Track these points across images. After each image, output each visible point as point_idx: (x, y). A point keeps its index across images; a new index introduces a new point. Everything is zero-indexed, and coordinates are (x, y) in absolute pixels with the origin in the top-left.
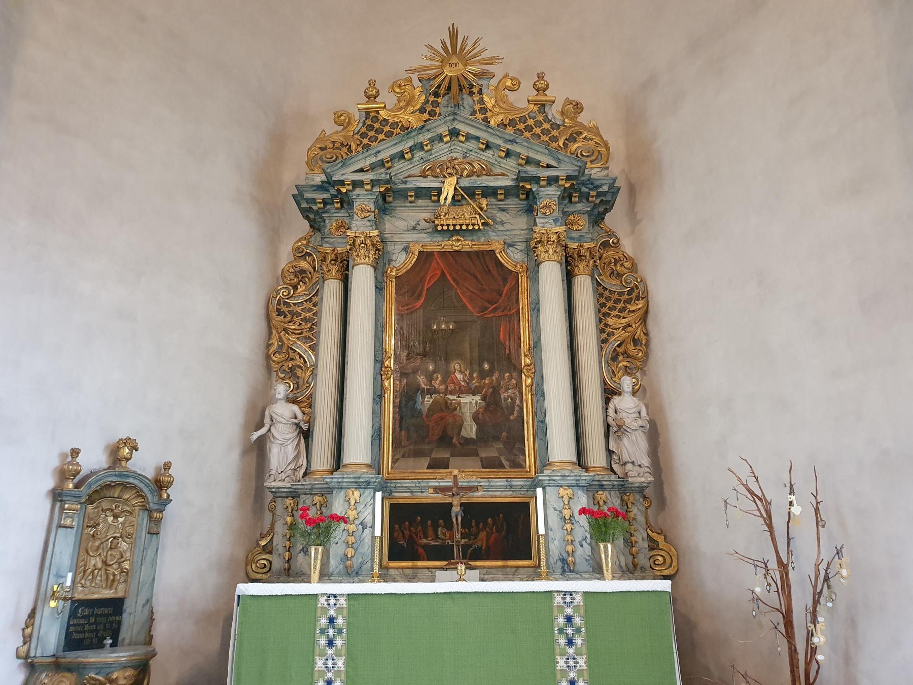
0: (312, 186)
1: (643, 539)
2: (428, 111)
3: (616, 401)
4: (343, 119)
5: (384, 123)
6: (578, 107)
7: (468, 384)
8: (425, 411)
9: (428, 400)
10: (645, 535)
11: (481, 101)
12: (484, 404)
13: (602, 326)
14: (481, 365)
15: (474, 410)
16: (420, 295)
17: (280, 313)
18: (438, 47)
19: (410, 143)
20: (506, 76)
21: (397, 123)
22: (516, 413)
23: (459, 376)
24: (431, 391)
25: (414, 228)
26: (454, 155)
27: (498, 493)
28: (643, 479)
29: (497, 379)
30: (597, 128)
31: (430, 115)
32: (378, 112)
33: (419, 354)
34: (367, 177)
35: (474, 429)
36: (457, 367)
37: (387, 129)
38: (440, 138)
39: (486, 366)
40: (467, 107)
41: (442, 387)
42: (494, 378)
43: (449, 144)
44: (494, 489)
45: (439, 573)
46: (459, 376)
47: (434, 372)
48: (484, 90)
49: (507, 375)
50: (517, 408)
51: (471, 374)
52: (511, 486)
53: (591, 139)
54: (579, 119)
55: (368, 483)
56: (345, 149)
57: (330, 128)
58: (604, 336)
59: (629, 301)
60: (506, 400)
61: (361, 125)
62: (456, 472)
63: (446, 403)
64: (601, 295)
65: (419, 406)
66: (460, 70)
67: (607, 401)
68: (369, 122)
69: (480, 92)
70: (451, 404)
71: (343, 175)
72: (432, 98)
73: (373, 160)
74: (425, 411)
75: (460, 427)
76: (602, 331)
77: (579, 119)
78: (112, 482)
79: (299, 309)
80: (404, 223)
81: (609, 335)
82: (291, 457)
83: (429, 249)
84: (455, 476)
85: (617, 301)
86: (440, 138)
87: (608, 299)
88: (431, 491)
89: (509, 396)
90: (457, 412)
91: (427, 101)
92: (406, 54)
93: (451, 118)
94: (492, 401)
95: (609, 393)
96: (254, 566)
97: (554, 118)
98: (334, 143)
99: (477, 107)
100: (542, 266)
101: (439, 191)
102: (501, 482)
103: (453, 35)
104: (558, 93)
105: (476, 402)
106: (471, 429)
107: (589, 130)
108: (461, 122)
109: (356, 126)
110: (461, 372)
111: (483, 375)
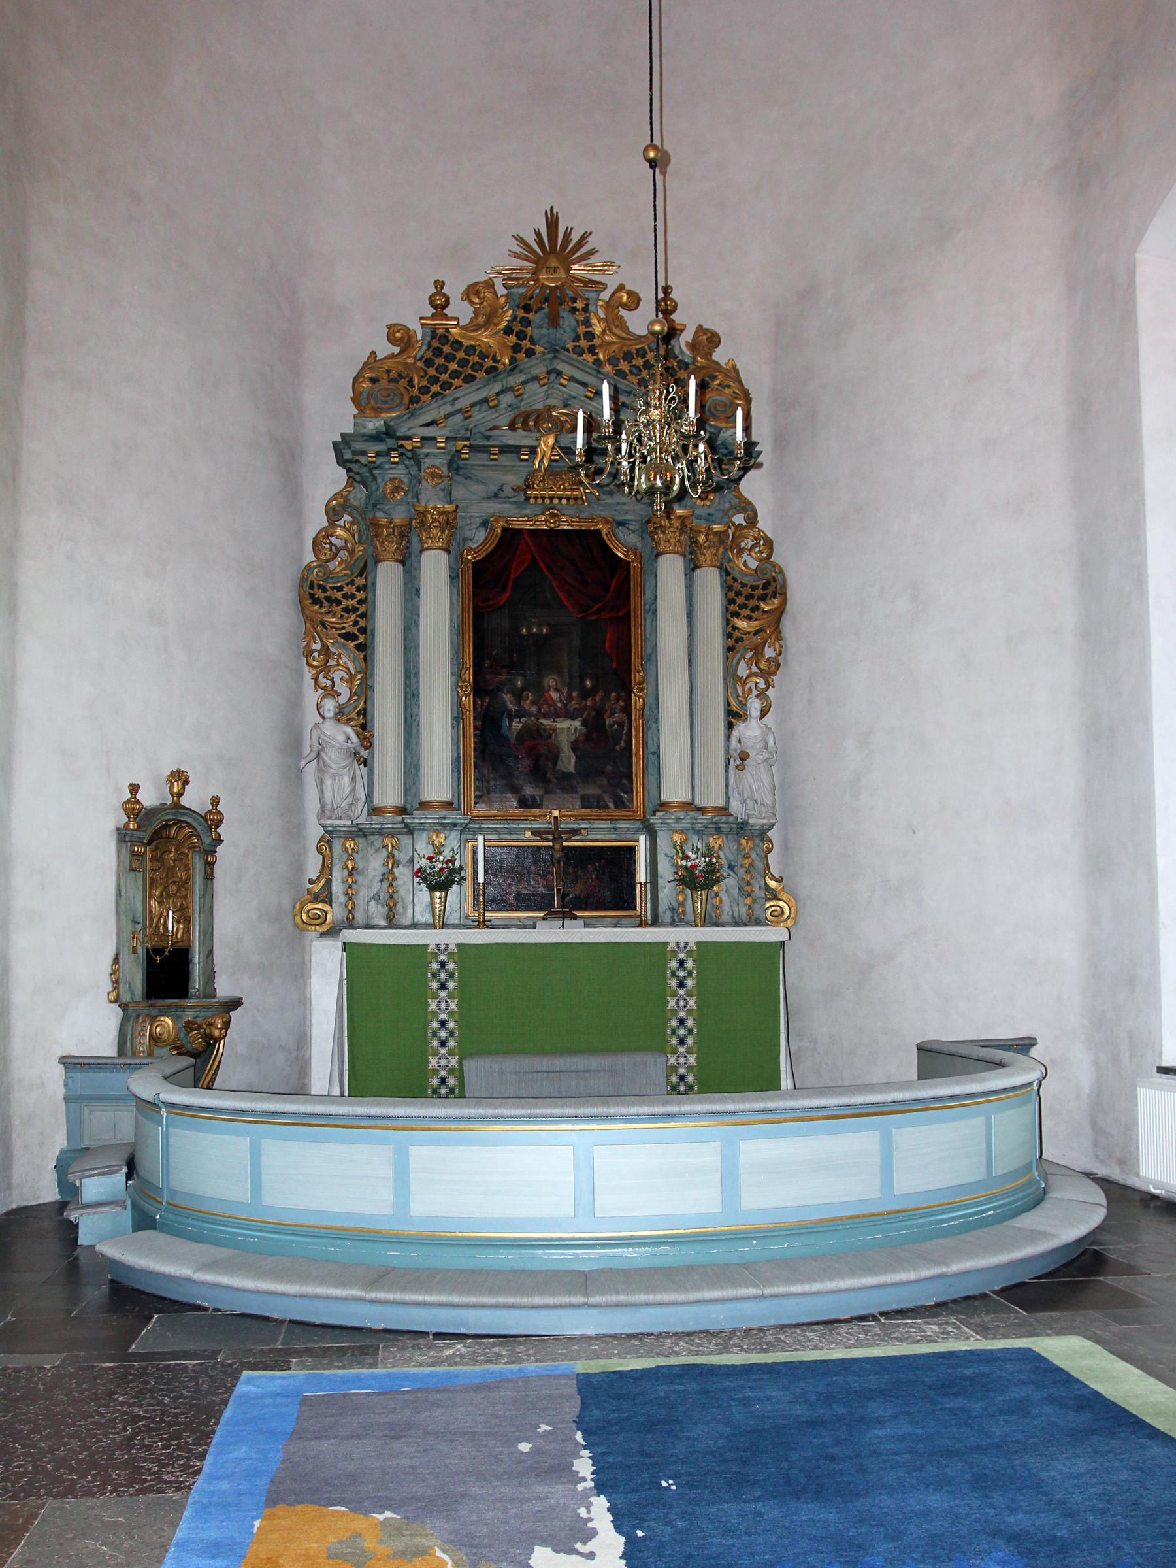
0: (363, 435)
1: (760, 888)
2: (518, 330)
3: (740, 729)
4: (398, 335)
5: (456, 346)
6: (714, 340)
7: (566, 705)
8: (513, 736)
9: (517, 725)
10: (763, 883)
11: (587, 322)
12: (584, 730)
13: (732, 595)
14: (582, 681)
15: (573, 738)
16: (504, 588)
17: (315, 600)
18: (531, 240)
19: (497, 388)
20: (621, 288)
21: (473, 347)
22: (622, 744)
23: (555, 695)
24: (520, 714)
25: (496, 496)
26: (550, 402)
27: (599, 837)
28: (765, 821)
29: (601, 700)
30: (737, 371)
31: (519, 338)
32: (447, 330)
33: (505, 667)
34: (442, 432)
35: (573, 761)
36: (552, 683)
37: (461, 355)
38: (536, 379)
39: (588, 683)
40: (568, 330)
41: (534, 709)
42: (597, 698)
43: (546, 387)
44: (597, 833)
45: (540, 923)
46: (555, 695)
47: (523, 689)
48: (592, 308)
49: (613, 694)
50: (624, 737)
51: (570, 694)
52: (615, 829)
53: (729, 387)
54: (715, 357)
55: (455, 825)
56: (403, 383)
57: (385, 349)
58: (731, 642)
59: (763, 598)
60: (611, 726)
61: (425, 347)
62: (556, 813)
63: (538, 731)
64: (730, 588)
65: (504, 730)
66: (561, 279)
67: (730, 726)
68: (435, 344)
69: (586, 309)
70: (545, 730)
71: (410, 429)
72: (521, 313)
73: (448, 409)
74: (513, 736)
75: (555, 759)
76: (729, 636)
77: (715, 357)
78: (169, 820)
79: (339, 595)
80: (482, 487)
81: (737, 641)
82: (347, 790)
83: (517, 525)
84: (556, 818)
85: (749, 597)
86: (536, 379)
87: (738, 594)
88: (528, 834)
89: (615, 722)
90: (552, 740)
91: (514, 318)
92: (490, 252)
93: (551, 355)
94: (595, 727)
95: (733, 716)
96: (304, 917)
97: (682, 352)
98: (388, 372)
99: (582, 330)
100: (662, 559)
101: (533, 450)
102: (605, 825)
103: (552, 222)
104: (688, 318)
105: (576, 729)
106: (569, 762)
107: (726, 373)
108: (563, 361)
109: (420, 350)
110: (556, 690)
111: (585, 694)
